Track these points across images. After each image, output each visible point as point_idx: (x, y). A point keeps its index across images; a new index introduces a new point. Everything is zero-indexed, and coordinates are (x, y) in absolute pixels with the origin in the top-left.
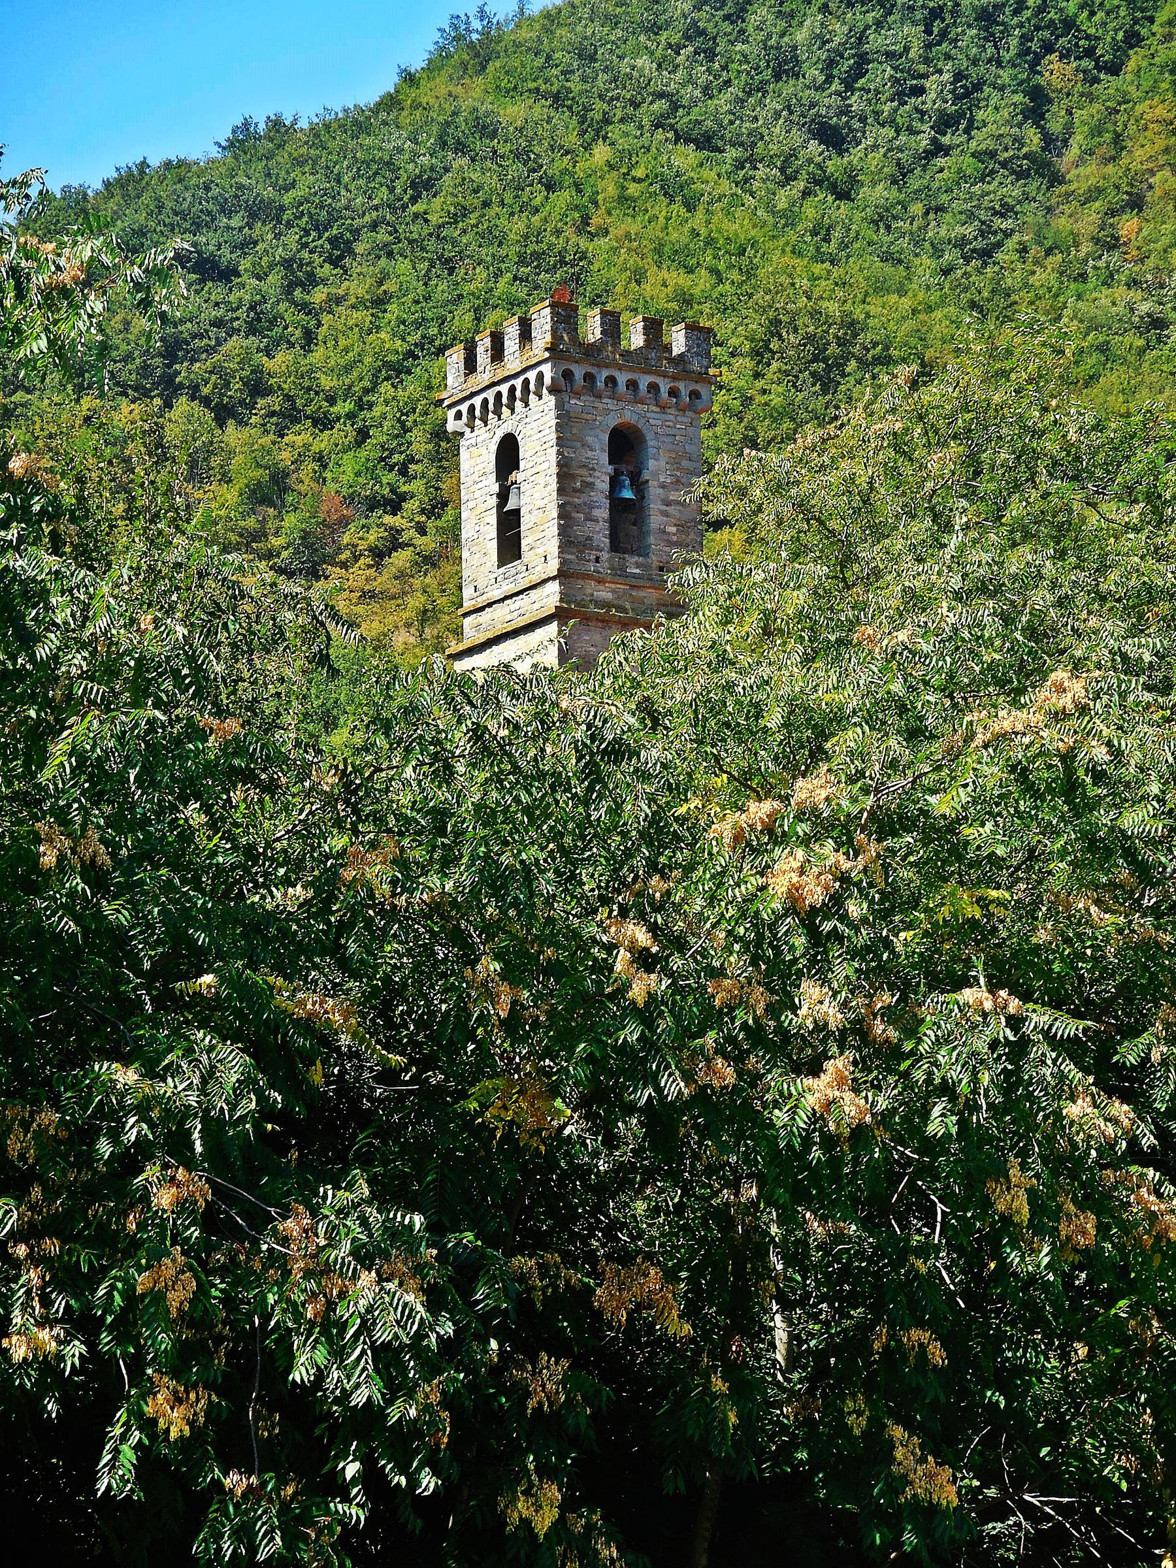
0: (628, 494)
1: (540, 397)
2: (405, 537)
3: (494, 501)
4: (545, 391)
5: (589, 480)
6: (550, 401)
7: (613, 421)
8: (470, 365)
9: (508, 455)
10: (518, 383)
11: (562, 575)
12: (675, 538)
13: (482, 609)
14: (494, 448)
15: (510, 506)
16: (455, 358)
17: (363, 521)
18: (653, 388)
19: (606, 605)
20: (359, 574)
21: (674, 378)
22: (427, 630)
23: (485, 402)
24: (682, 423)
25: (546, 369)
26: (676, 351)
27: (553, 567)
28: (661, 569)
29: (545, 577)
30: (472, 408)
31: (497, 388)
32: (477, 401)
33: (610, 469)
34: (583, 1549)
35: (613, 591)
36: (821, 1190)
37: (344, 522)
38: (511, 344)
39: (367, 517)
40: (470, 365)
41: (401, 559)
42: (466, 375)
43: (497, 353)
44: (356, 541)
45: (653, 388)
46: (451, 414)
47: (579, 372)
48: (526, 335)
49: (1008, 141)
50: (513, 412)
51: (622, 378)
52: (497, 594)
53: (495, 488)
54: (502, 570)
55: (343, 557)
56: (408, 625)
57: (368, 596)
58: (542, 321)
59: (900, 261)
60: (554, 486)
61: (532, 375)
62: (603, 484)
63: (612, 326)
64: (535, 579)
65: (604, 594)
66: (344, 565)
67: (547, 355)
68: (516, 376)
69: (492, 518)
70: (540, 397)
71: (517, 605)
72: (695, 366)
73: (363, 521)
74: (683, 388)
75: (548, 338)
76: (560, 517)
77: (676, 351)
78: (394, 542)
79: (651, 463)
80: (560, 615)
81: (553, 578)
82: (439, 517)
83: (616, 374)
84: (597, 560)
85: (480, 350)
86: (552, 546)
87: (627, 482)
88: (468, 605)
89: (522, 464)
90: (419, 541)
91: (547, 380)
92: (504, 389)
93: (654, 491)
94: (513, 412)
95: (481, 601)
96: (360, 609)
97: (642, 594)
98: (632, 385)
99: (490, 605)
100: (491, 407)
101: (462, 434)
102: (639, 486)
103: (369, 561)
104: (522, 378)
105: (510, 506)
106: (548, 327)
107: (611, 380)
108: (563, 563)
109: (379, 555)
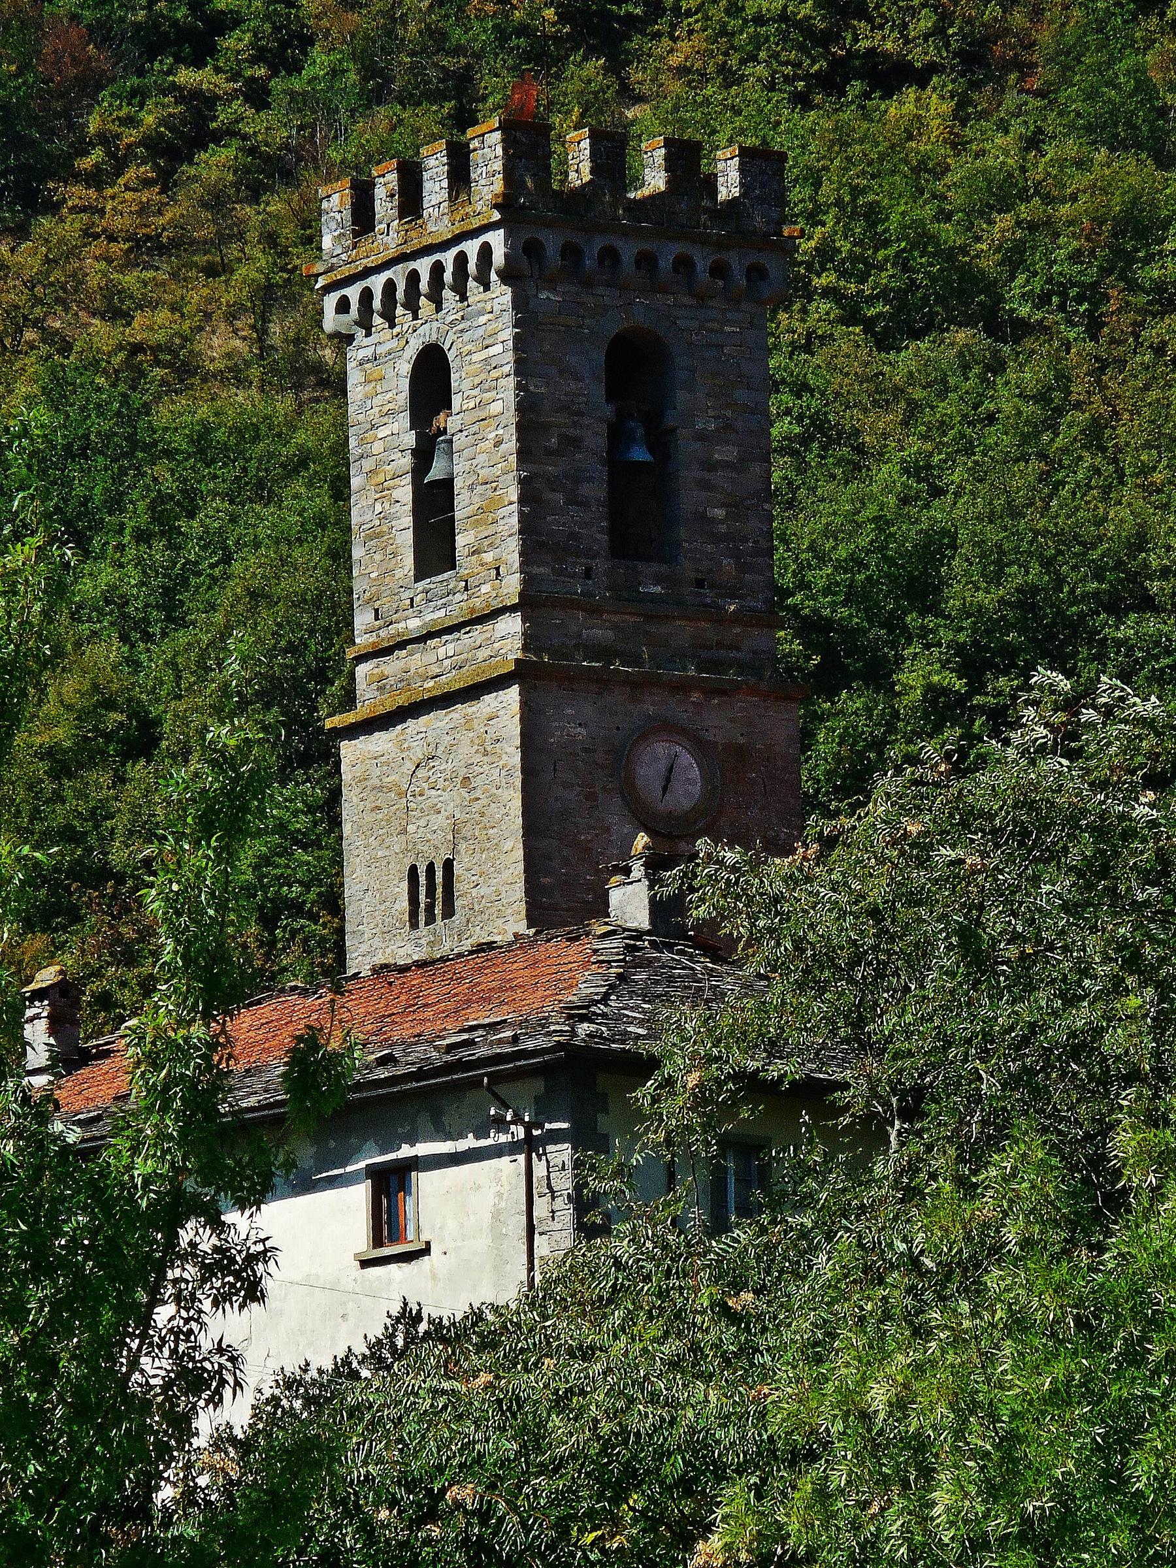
0: (640, 454)
1: (487, 287)
2: (223, 116)
3: (406, 462)
4: (494, 277)
5: (572, 432)
6: (502, 296)
7: (613, 326)
8: (363, 219)
9: (431, 380)
10: (448, 258)
11: (527, 604)
12: (723, 528)
13: (387, 651)
14: (405, 368)
15: (436, 472)
16: (336, 203)
17: (134, 81)
18: (684, 264)
19: (604, 653)
20: (122, 203)
21: (721, 245)
22: (275, 328)
23: (390, 286)
24: (733, 323)
25: (497, 239)
26: (723, 194)
27: (512, 585)
28: (699, 583)
29: (496, 604)
30: (367, 295)
31: (413, 265)
32: (377, 283)
33: (608, 411)
37: (90, 85)
38: (435, 189)
39: (141, 73)
40: (363, 219)
41: (215, 164)
42: (356, 234)
43: (410, 202)
44: (115, 128)
45: (684, 264)
46: (330, 301)
47: (552, 241)
48: (460, 177)
50: (439, 309)
51: (628, 251)
52: (414, 625)
53: (410, 439)
54: (421, 585)
55: (86, 163)
56: (231, 316)
57: (145, 247)
58: (489, 153)
60: (511, 445)
61: (471, 248)
62: (596, 439)
63: (613, 154)
65: (600, 633)
66: (96, 179)
67: (496, 216)
68: (444, 246)
69: (405, 492)
70: (487, 287)
71: (450, 649)
72: (759, 222)
73: (134, 81)
74: (736, 262)
75: (498, 186)
76: (522, 500)
77: (723, 194)
78: (196, 128)
79: (681, 397)
80: (521, 674)
82: (295, 68)
83: (619, 244)
84: (588, 573)
85: (380, 192)
86: (511, 552)
87: (640, 432)
89: (456, 401)
90: (255, 124)
91: (498, 257)
92: (423, 266)
93: (686, 446)
94: (439, 309)
96: (129, 280)
98: (646, 261)
99: (401, 645)
100: (400, 294)
101: (350, 339)
102: (661, 441)
103: (146, 170)
104: (454, 251)
105: (436, 472)
106: (498, 166)
107: (610, 255)
108: (528, 581)
109: (172, 152)
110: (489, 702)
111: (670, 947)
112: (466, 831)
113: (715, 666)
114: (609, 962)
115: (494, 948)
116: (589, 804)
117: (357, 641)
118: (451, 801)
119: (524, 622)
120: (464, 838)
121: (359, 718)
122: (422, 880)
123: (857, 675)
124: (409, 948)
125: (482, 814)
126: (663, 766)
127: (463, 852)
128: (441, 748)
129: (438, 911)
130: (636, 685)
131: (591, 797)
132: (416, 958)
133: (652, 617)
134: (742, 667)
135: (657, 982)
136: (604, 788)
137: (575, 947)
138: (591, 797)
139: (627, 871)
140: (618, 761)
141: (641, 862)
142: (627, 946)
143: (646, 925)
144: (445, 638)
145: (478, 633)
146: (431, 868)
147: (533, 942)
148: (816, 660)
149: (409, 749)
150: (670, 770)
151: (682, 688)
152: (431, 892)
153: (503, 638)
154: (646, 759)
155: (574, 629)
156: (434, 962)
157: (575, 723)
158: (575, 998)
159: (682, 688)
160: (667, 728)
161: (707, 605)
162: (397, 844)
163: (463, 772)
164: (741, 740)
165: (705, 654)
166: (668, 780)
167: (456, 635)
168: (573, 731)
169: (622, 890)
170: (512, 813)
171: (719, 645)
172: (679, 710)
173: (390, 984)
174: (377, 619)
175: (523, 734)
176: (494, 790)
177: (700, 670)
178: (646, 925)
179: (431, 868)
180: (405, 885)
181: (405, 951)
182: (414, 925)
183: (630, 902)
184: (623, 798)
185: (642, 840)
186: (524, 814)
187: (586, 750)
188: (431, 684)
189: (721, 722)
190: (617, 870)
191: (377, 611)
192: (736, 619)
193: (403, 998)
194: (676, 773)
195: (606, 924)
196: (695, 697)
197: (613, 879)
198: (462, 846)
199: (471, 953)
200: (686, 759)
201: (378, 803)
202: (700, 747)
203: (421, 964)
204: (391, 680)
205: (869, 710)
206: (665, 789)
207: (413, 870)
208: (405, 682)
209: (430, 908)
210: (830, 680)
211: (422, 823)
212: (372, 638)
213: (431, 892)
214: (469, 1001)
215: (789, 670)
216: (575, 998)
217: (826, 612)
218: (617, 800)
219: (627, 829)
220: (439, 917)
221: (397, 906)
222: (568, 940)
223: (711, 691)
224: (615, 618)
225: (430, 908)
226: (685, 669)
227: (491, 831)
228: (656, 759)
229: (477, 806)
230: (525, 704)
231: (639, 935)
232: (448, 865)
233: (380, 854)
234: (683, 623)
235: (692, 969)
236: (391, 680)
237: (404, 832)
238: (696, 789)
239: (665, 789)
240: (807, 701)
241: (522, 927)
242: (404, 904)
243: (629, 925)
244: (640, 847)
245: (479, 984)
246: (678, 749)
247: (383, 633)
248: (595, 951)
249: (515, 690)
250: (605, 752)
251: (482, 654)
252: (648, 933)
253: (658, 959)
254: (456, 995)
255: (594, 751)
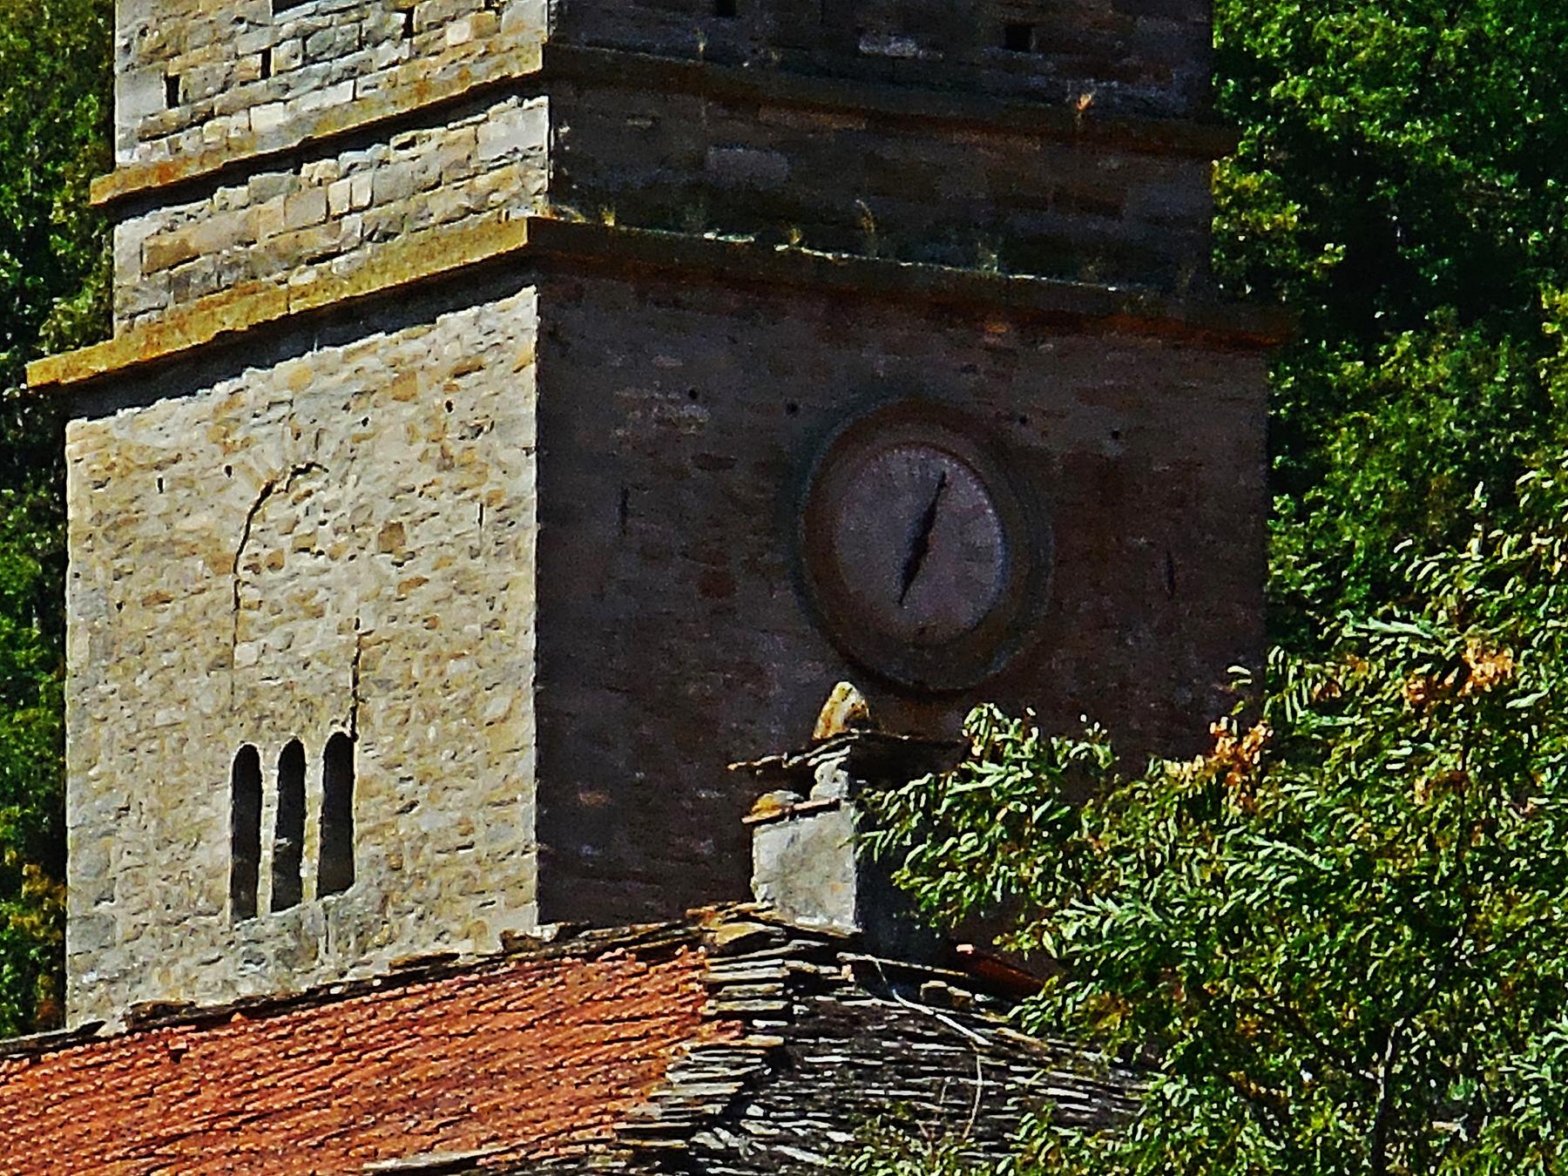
13: (199, 188)
29: (486, 74)
34: (762, 5)
36: (1171, 1118)
52: (270, 123)
64: (442, 77)
81: (526, 87)
88: (133, 159)
95: (197, 150)
99: (236, 174)
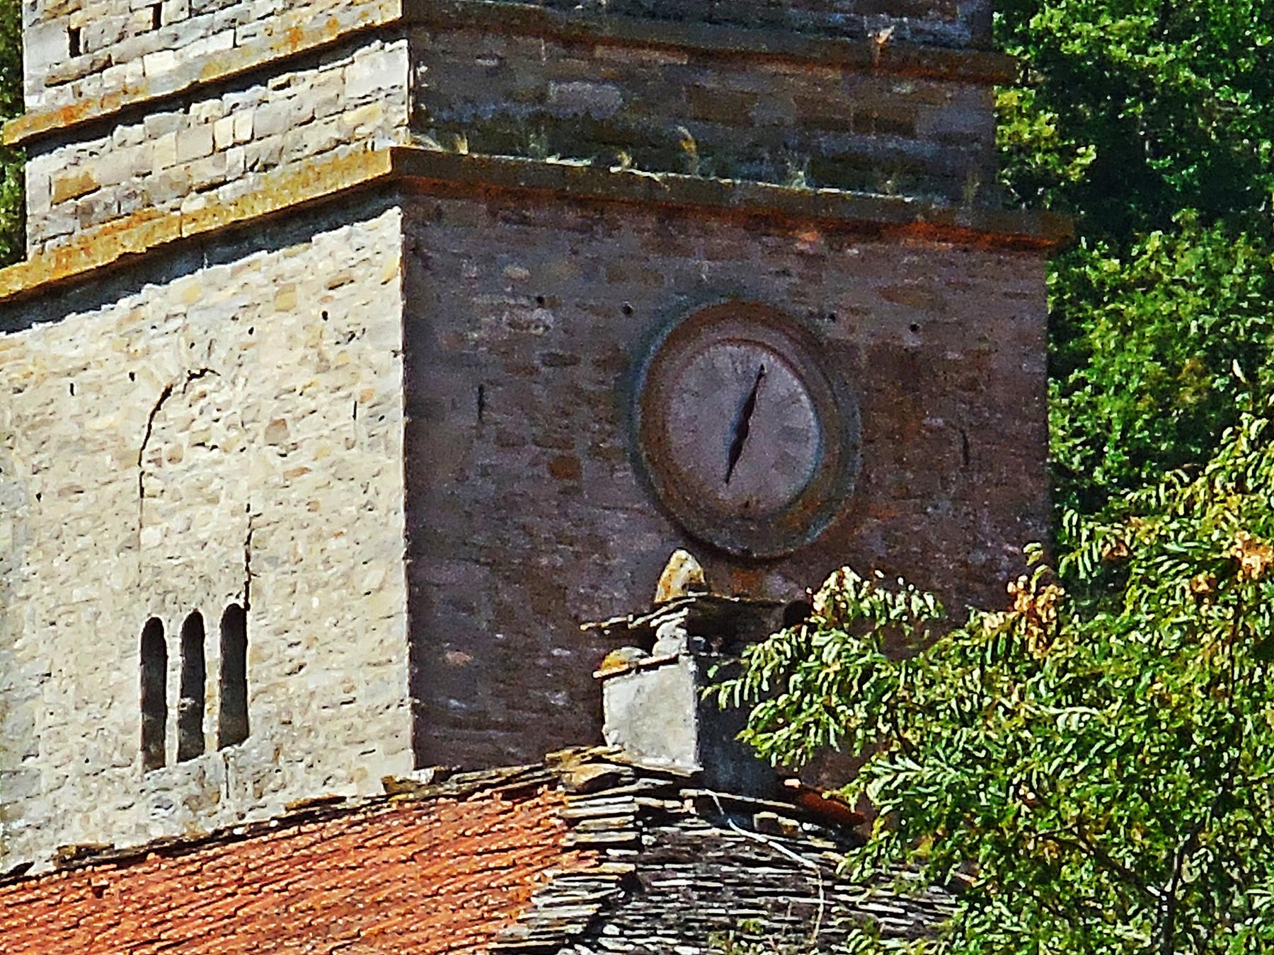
13: (100, 128)
19: (596, 136)
35: (626, 78)
49: (240, 790)
52: (162, 70)
59: (203, 372)
65: (587, 92)
71: (244, 123)
81: (388, 33)
88: (42, 104)
95: (98, 94)
97: (739, 83)
99: (133, 114)
110: (331, 246)
111: (743, 813)
112: (276, 544)
113: (852, 169)
114: (602, 847)
115: (338, 814)
116: (557, 486)
117: (30, 101)
118: (244, 476)
119: (414, 63)
120: (273, 561)
121: (33, 281)
122: (175, 655)
123: (1187, 197)
124: (142, 811)
125: (313, 507)
126: (730, 400)
127: (268, 591)
128: (220, 352)
129: (210, 725)
130: (672, 213)
131: (564, 469)
132: (157, 833)
133: (709, 55)
134: (915, 174)
135: (711, 895)
136: (595, 451)
137: (522, 813)
138: (564, 469)
139: (646, 639)
140: (631, 388)
141: (678, 618)
142: (645, 809)
143: (688, 764)
144: (230, 98)
145: (308, 86)
146: (194, 627)
147: (426, 804)
148: (1089, 155)
149: (147, 352)
150: (748, 407)
151: (773, 219)
152: (549, 933)
153: (365, 101)
154: (691, 380)
155: (526, 82)
156: (198, 843)
157: (535, 292)
158: (523, 931)
159: (773, 219)
160: (744, 310)
161: (834, 31)
162: (116, 571)
163: (270, 409)
164: (912, 341)
165: (825, 141)
166: (742, 430)
167: (256, 92)
168: (525, 316)
169: (635, 681)
170: (381, 503)
171: (863, 122)
172: (766, 270)
173: (99, 892)
174: (74, 52)
175: (409, 320)
176: (340, 452)
177: (817, 178)
178: (688, 764)
179: (194, 627)
180: (134, 667)
181: (130, 820)
182: (155, 760)
183: (652, 711)
184: (639, 471)
185: (683, 567)
186: (410, 506)
187: (553, 360)
188: (194, 204)
189: (868, 301)
190: (621, 636)
191: (75, 34)
192: (899, 60)
193: (127, 925)
194: (754, 415)
195: (598, 759)
196: (808, 240)
197: (613, 656)
198: (267, 579)
199: (285, 823)
200: (783, 382)
201: (76, 479)
202: (816, 354)
203: (171, 849)
204: (106, 195)
205: (1214, 276)
206: (735, 453)
207: (154, 630)
208: (142, 204)
209: (191, 721)
210: (1120, 202)
211: (177, 523)
212: (65, 97)
213: (549, 933)
214: (277, 933)
215: (1027, 183)
216: (523, 931)
217: (1121, 52)
218: (625, 474)
219: (647, 542)
220: (211, 739)
221: (115, 715)
222: (508, 795)
223: (842, 230)
224: (622, 56)
225: (191, 721)
226: (783, 176)
227: (333, 544)
228: (714, 381)
229: (301, 489)
230: (413, 253)
231: (673, 785)
232: (235, 620)
233: (77, 594)
234: (784, 69)
235: (794, 865)
236: (106, 195)
237: (132, 546)
238: (809, 455)
239: (735, 453)
240: (1064, 253)
241: (403, 766)
242: (131, 711)
243: (648, 762)
244: (676, 585)
245: (304, 893)
246: (765, 359)
247: (89, 86)
248: (572, 822)
249: (393, 216)
250: (598, 364)
251: (318, 135)
252: (695, 781)
253: (715, 843)
254: (250, 919)
255: (574, 361)
